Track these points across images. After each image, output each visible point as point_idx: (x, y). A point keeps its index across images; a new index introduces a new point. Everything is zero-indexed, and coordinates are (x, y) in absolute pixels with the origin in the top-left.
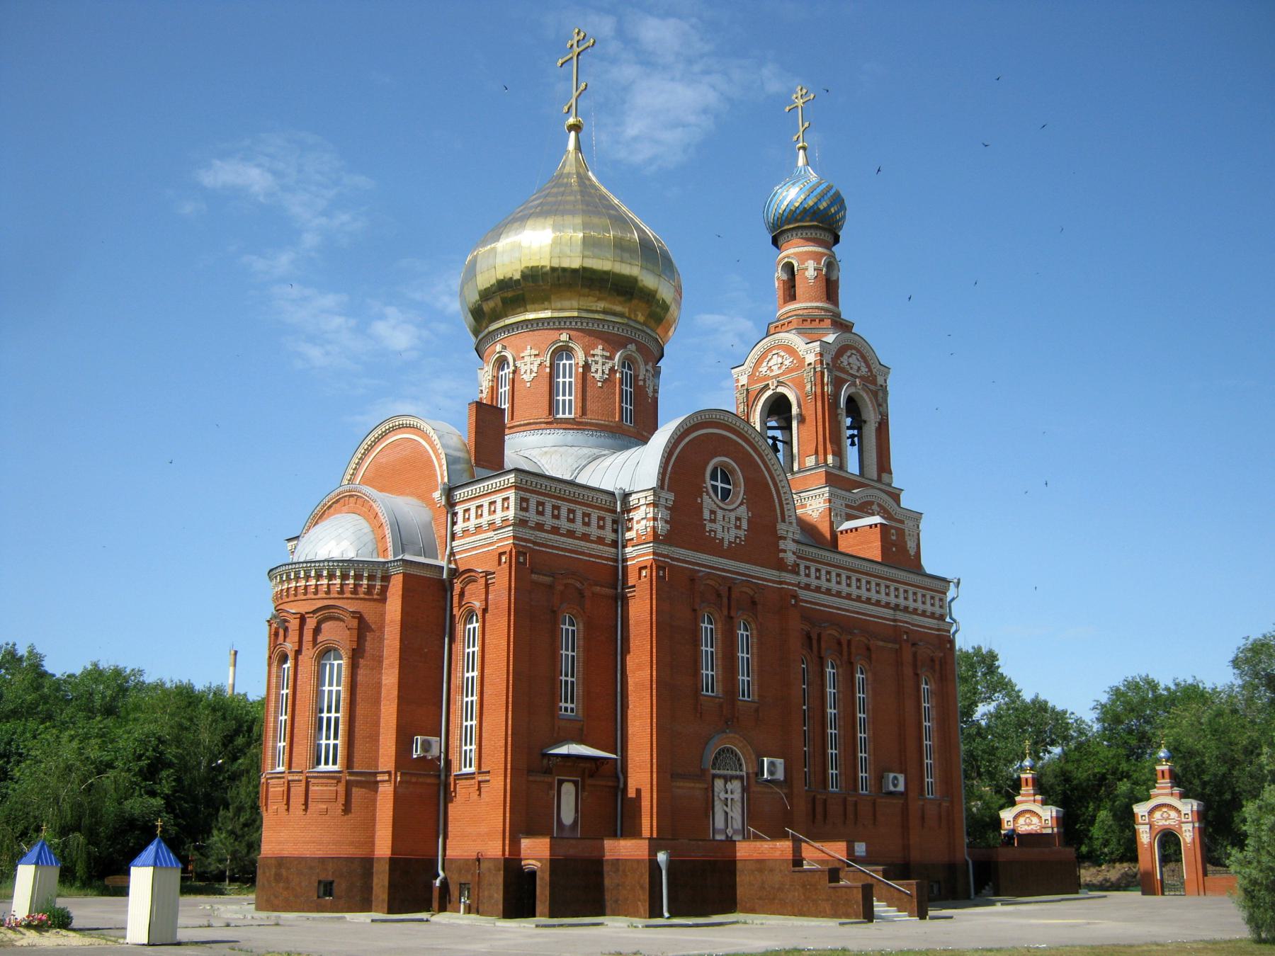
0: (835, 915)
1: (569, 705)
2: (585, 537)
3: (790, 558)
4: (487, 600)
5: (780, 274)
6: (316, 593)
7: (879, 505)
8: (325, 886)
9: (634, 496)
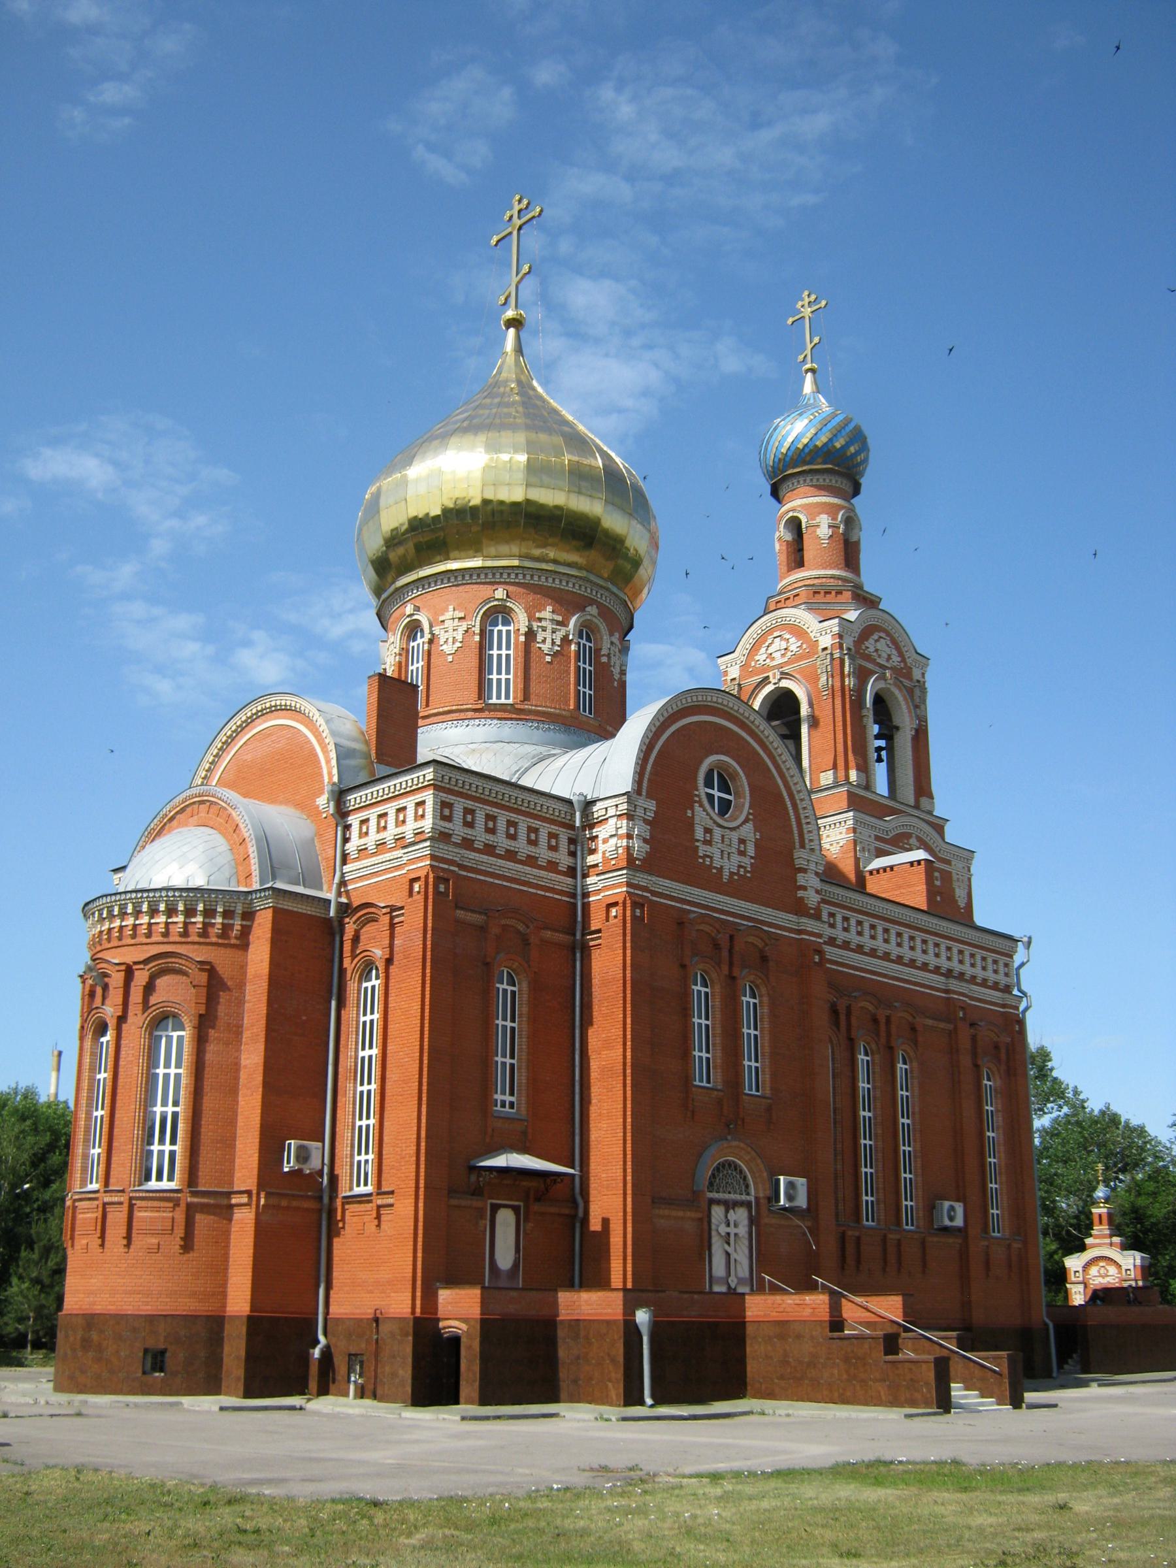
0: (894, 1402)
1: (508, 1098)
2: (531, 861)
3: (812, 898)
4: (391, 946)
5: (783, 533)
6: (149, 935)
7: (919, 839)
8: (155, 1357)
9: (599, 805)
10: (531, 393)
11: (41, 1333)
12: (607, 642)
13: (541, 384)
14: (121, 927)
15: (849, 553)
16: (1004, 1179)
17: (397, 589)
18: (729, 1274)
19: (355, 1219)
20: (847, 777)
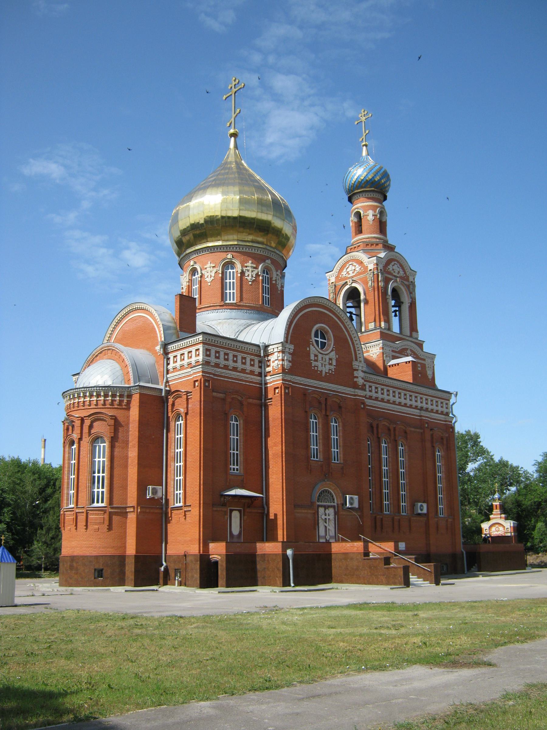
0: (388, 584)
1: (236, 467)
2: (243, 371)
3: (360, 381)
4: (187, 408)
5: (353, 218)
6: (90, 405)
7: (411, 350)
9: (271, 347)
10: (241, 167)
11: (48, 564)
12: (275, 274)
13: (245, 162)
14: (78, 402)
15: (382, 226)
16: (445, 493)
17: (186, 254)
18: (326, 535)
19: (176, 516)
20: (380, 325)
